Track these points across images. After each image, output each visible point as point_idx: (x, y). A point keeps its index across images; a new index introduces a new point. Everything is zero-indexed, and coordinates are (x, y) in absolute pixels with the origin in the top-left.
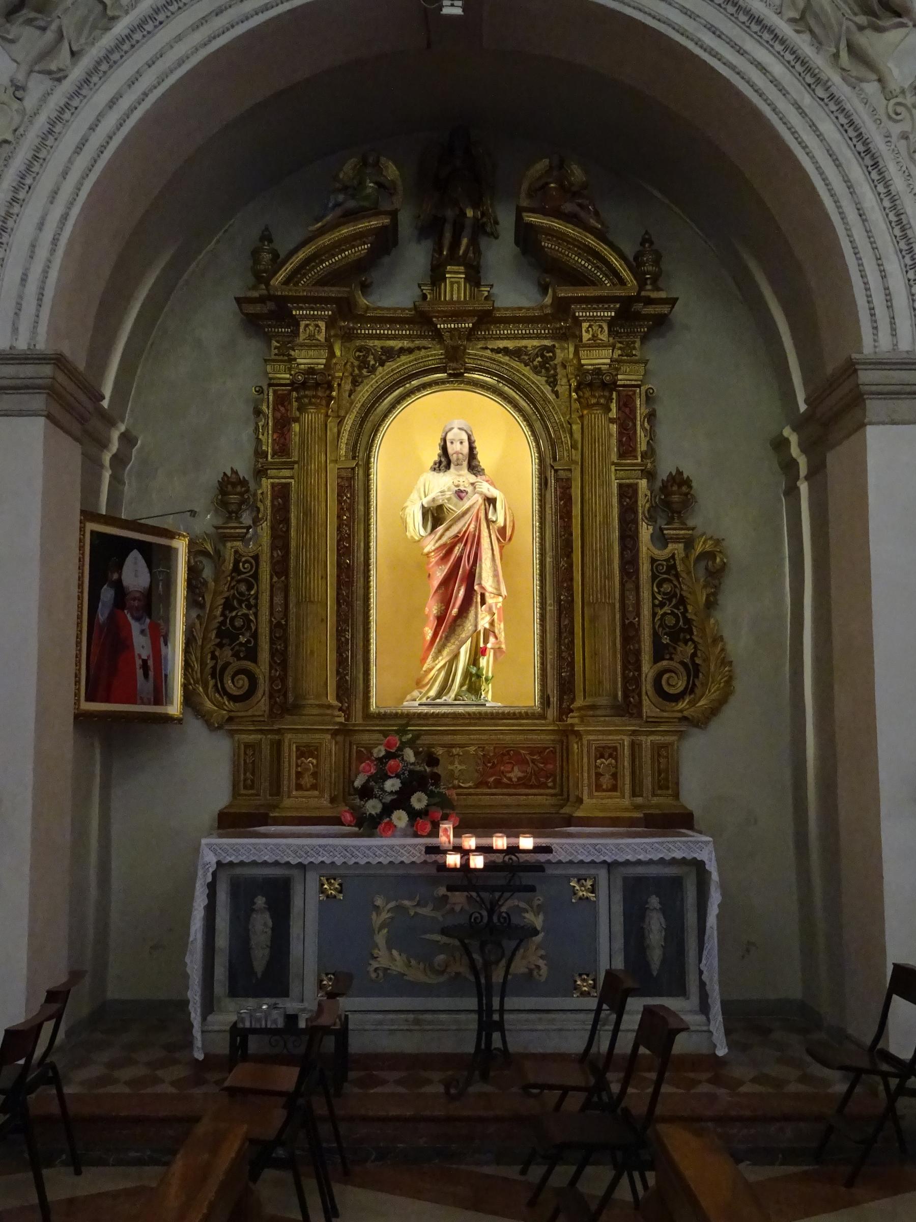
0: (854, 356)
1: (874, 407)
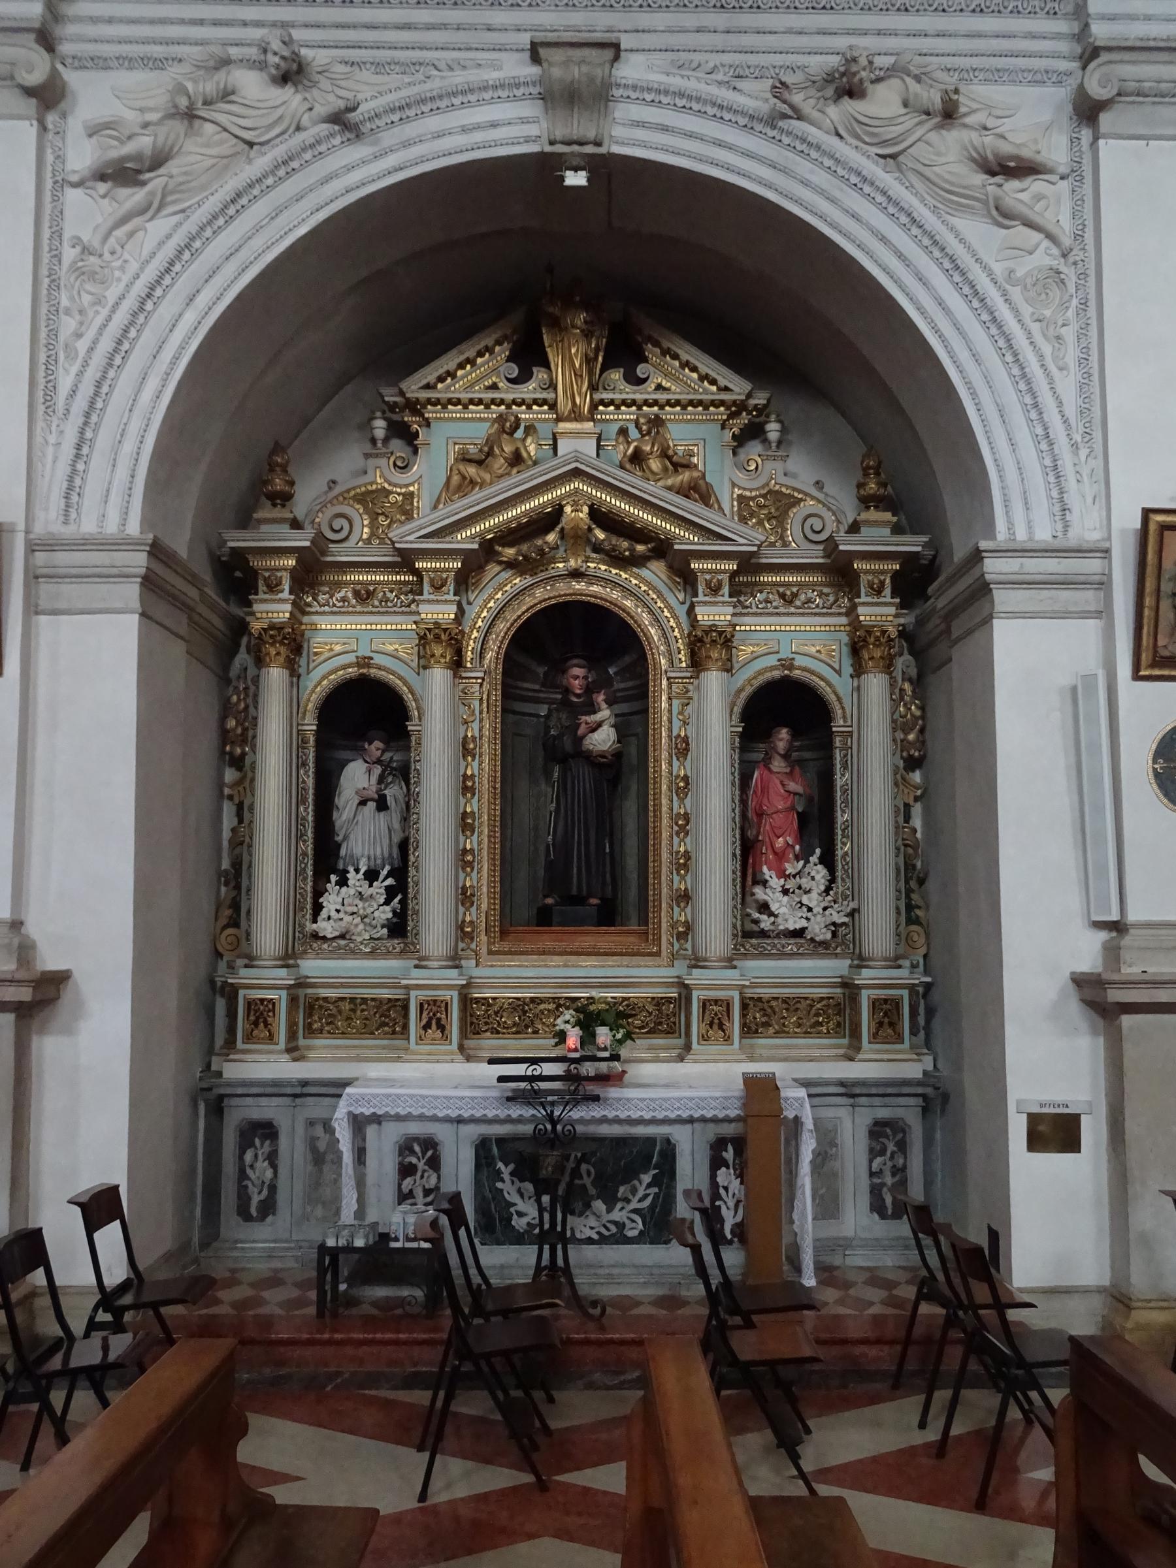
0: (983, 545)
1: (1002, 598)
